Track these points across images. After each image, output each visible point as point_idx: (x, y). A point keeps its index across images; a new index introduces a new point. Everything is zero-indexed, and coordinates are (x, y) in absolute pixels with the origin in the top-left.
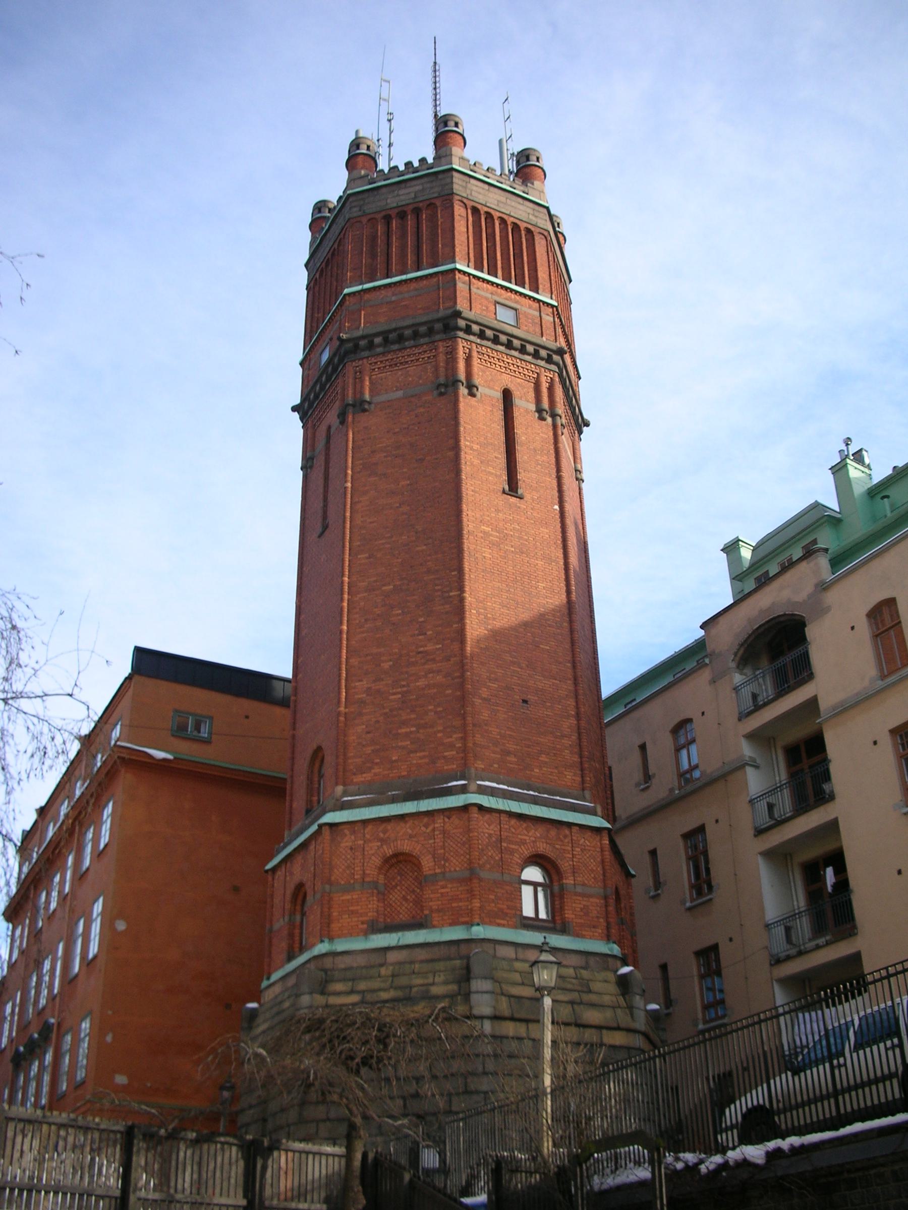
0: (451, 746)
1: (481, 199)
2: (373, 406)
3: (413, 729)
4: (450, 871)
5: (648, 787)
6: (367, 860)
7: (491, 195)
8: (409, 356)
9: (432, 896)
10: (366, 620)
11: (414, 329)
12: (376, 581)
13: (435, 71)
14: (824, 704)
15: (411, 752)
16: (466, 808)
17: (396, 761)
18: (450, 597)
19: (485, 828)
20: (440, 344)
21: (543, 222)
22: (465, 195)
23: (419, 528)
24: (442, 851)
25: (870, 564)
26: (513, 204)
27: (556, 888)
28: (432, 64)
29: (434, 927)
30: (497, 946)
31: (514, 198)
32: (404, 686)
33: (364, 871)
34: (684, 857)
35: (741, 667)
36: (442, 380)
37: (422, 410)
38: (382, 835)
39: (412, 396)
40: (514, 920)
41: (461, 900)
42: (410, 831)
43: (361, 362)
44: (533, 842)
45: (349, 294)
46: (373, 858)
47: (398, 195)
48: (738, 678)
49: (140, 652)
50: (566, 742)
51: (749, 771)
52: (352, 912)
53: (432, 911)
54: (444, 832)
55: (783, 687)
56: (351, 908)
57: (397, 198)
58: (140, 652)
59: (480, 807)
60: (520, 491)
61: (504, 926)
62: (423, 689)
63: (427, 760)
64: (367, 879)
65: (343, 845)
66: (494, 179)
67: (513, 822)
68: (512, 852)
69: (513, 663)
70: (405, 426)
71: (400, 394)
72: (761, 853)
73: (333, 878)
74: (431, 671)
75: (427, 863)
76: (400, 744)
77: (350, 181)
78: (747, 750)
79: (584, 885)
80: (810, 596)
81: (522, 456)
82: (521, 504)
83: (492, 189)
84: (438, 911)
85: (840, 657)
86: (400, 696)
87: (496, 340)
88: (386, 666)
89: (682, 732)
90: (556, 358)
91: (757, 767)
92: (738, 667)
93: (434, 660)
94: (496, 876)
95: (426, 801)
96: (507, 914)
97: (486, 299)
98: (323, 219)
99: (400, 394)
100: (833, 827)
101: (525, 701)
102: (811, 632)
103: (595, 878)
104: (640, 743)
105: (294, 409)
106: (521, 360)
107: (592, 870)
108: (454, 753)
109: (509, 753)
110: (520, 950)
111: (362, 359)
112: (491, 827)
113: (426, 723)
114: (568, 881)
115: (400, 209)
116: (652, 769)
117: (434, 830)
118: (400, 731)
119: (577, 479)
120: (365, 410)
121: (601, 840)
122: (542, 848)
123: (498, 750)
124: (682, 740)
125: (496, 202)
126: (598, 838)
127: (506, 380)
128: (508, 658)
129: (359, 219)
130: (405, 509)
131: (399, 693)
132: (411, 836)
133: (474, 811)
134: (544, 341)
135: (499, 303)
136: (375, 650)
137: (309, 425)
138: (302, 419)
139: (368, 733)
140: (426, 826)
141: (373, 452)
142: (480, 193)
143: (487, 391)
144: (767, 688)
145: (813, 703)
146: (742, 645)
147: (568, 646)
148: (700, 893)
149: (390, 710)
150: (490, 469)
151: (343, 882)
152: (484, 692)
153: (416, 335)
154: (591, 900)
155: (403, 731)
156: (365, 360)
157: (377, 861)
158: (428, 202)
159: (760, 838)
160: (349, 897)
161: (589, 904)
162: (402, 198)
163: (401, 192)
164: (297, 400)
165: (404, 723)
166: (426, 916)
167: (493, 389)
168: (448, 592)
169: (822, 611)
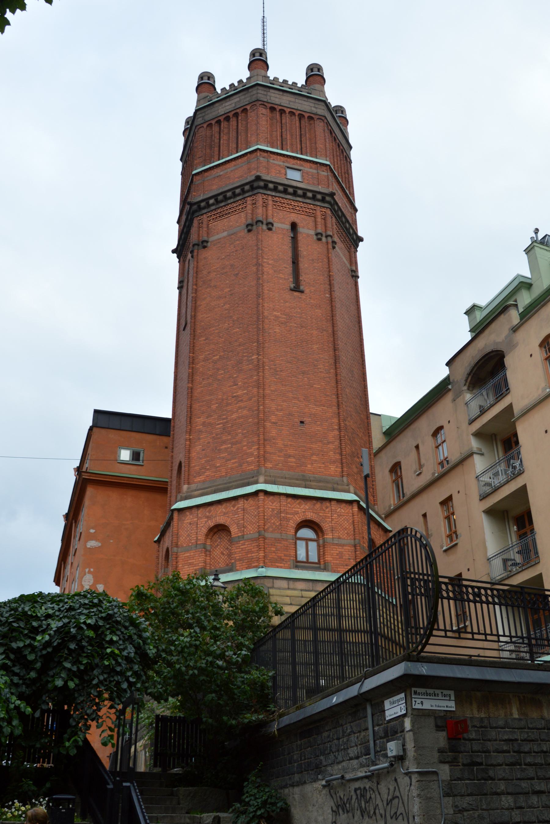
0: (252, 454)
1: (277, 101)
2: (209, 244)
3: (230, 445)
4: (247, 534)
5: (420, 473)
6: (199, 531)
7: (284, 98)
8: (230, 209)
9: (236, 550)
10: (203, 379)
11: (305, 192)
12: (209, 354)
13: (263, 22)
14: (517, 410)
15: (229, 460)
16: (256, 493)
17: (219, 467)
18: (253, 359)
19: (271, 505)
20: (249, 198)
21: (322, 111)
22: (265, 100)
23: (235, 318)
24: (242, 522)
25: (539, 312)
26: (300, 102)
27: (321, 542)
28: (261, 18)
29: (237, 570)
30: (275, 581)
31: (301, 98)
32: (224, 419)
33: (197, 537)
34: (442, 518)
35: (471, 389)
36: (249, 221)
37: (238, 242)
38: (207, 514)
39: (232, 234)
40: (289, 563)
41: (252, 552)
42: (224, 510)
43: (202, 217)
44: (304, 512)
45: (196, 174)
46: (203, 529)
47: (225, 107)
48: (468, 396)
49: (97, 413)
50: (331, 446)
51: (476, 457)
52: (190, 564)
53: (236, 560)
54: (244, 510)
55: (498, 399)
56: (189, 561)
57: (224, 108)
58: (97, 413)
59: (266, 493)
60: (302, 288)
61: (281, 567)
62: (235, 420)
63: (236, 465)
64: (199, 543)
65: (185, 522)
66: (287, 87)
67: (289, 500)
68: (288, 520)
69: (295, 398)
70: (228, 254)
71: (225, 234)
72: (484, 511)
73: (179, 543)
74: (240, 408)
75: (234, 530)
76: (222, 455)
77: (198, 101)
78: (475, 444)
79: (339, 538)
80: (506, 337)
81: (304, 265)
82: (303, 296)
83: (285, 94)
84: (240, 560)
85: (524, 375)
86: (222, 425)
87: (285, 192)
88: (214, 407)
89: (439, 436)
90: (328, 198)
91: (482, 454)
92: (468, 389)
93: (242, 400)
94: (277, 536)
95: (234, 490)
96: (283, 560)
97: (280, 166)
98: (192, 128)
99: (225, 234)
100: (523, 490)
101: (302, 422)
102: (508, 361)
103: (347, 533)
104: (416, 445)
105: (173, 252)
106: (303, 203)
107: (346, 529)
108: (253, 458)
109: (290, 456)
110: (291, 583)
111: (202, 215)
112: (274, 505)
113: (237, 441)
114: (328, 537)
115: (226, 115)
116: (423, 461)
117: (238, 509)
118: (221, 447)
119: (353, 276)
120: (205, 247)
121: (352, 508)
122: (310, 516)
123: (282, 454)
124: (439, 441)
125: (288, 102)
126: (350, 507)
127: (294, 217)
128: (291, 395)
129: (202, 125)
130: (227, 306)
131: (221, 423)
132: (225, 514)
133: (261, 496)
134: (320, 189)
135: (288, 167)
136: (208, 398)
137: (181, 259)
138: (178, 257)
139: (203, 450)
140: (234, 507)
141: (209, 273)
142: (276, 97)
143: (280, 225)
144: (491, 399)
145: (510, 408)
146: (469, 374)
147: (333, 384)
148: (451, 540)
149: (217, 435)
150: (281, 275)
151: (185, 545)
152: (273, 419)
153: (235, 195)
154: (345, 548)
155: (223, 447)
156: (205, 215)
157: (205, 530)
158: (242, 108)
159: (484, 501)
160: (189, 554)
161: (343, 550)
162: (227, 108)
163: (227, 104)
164: (174, 246)
165: (224, 442)
166: (232, 563)
167: (284, 223)
168: (251, 357)
169: (513, 346)
